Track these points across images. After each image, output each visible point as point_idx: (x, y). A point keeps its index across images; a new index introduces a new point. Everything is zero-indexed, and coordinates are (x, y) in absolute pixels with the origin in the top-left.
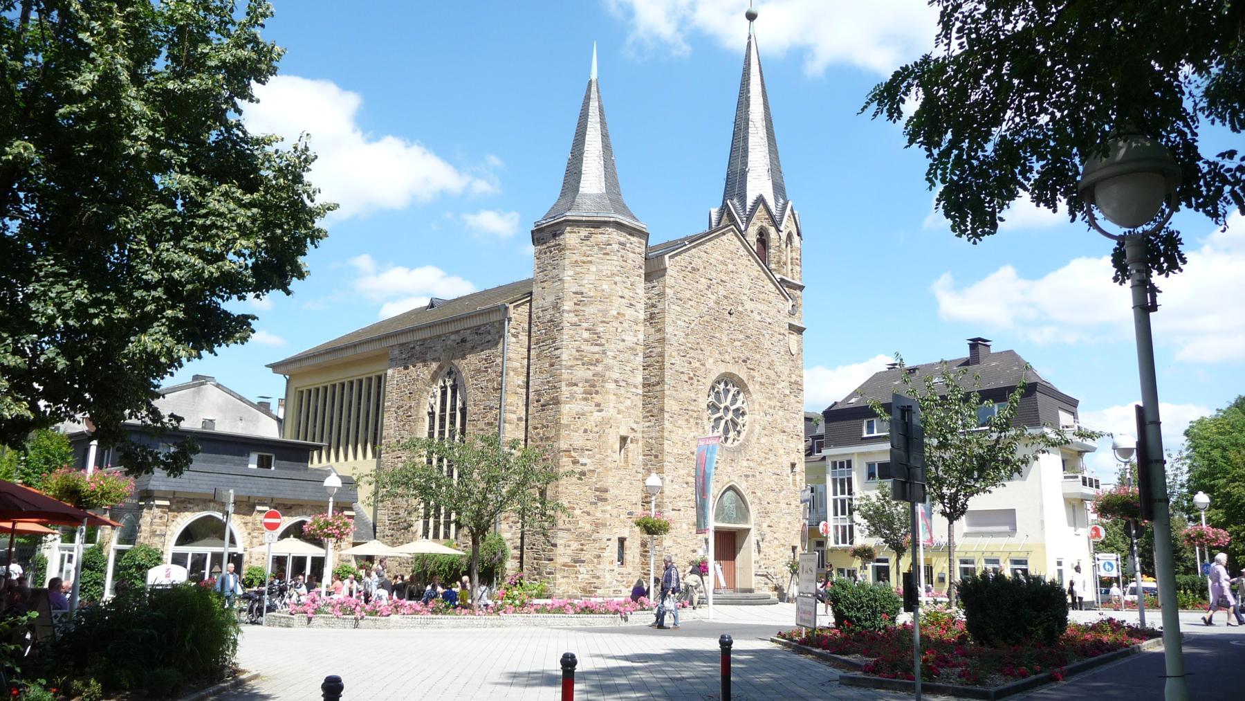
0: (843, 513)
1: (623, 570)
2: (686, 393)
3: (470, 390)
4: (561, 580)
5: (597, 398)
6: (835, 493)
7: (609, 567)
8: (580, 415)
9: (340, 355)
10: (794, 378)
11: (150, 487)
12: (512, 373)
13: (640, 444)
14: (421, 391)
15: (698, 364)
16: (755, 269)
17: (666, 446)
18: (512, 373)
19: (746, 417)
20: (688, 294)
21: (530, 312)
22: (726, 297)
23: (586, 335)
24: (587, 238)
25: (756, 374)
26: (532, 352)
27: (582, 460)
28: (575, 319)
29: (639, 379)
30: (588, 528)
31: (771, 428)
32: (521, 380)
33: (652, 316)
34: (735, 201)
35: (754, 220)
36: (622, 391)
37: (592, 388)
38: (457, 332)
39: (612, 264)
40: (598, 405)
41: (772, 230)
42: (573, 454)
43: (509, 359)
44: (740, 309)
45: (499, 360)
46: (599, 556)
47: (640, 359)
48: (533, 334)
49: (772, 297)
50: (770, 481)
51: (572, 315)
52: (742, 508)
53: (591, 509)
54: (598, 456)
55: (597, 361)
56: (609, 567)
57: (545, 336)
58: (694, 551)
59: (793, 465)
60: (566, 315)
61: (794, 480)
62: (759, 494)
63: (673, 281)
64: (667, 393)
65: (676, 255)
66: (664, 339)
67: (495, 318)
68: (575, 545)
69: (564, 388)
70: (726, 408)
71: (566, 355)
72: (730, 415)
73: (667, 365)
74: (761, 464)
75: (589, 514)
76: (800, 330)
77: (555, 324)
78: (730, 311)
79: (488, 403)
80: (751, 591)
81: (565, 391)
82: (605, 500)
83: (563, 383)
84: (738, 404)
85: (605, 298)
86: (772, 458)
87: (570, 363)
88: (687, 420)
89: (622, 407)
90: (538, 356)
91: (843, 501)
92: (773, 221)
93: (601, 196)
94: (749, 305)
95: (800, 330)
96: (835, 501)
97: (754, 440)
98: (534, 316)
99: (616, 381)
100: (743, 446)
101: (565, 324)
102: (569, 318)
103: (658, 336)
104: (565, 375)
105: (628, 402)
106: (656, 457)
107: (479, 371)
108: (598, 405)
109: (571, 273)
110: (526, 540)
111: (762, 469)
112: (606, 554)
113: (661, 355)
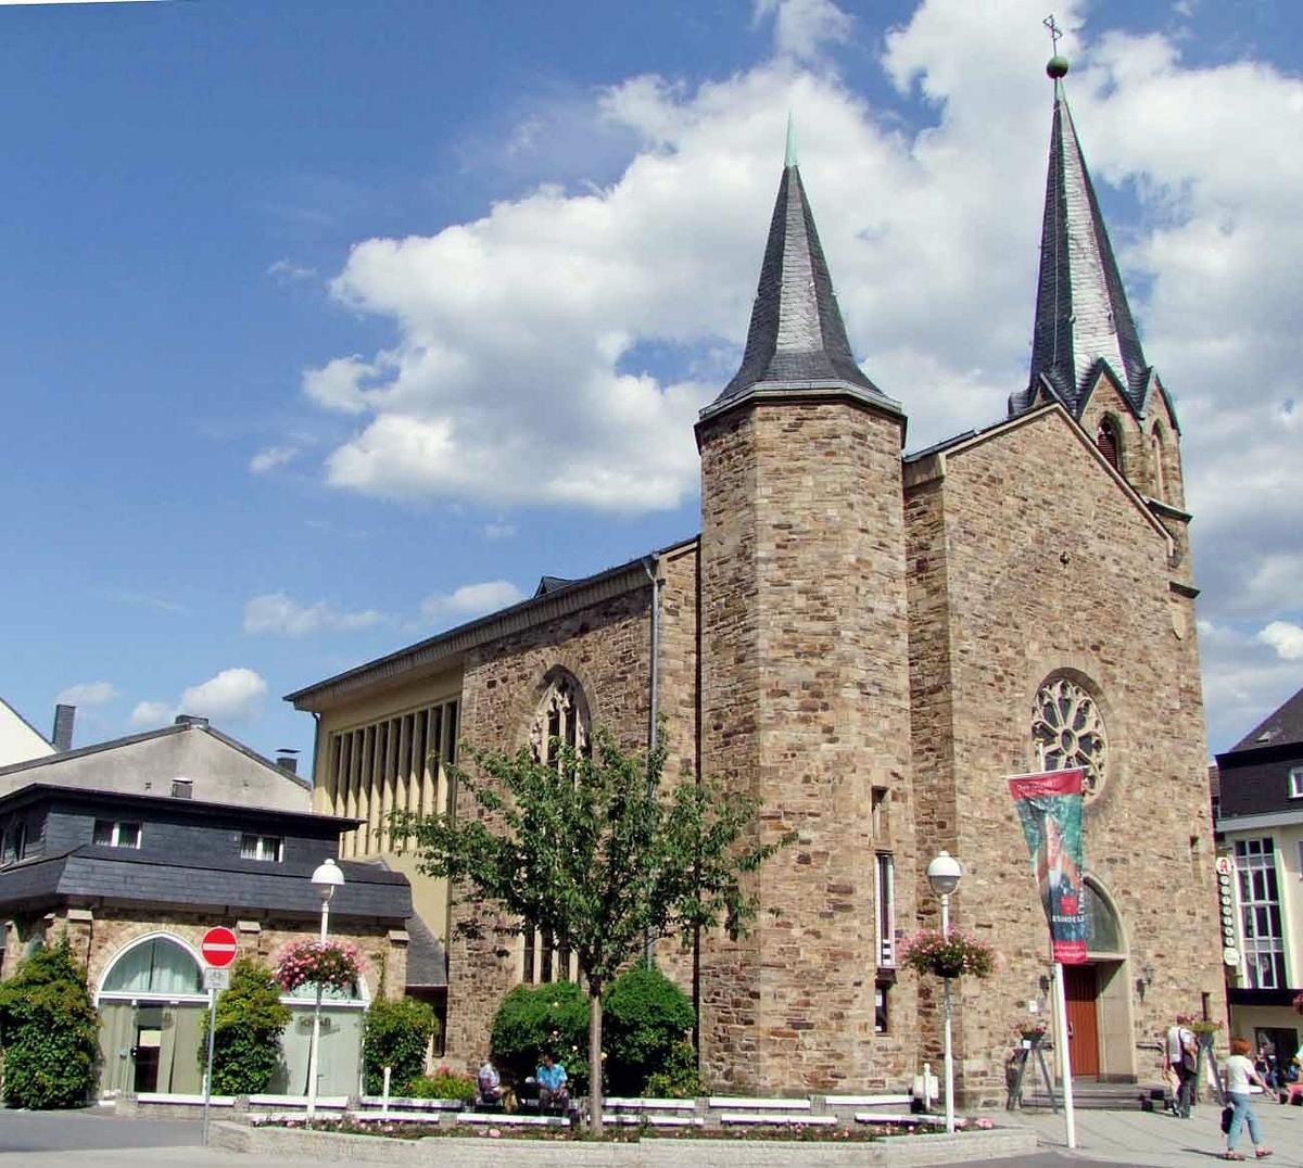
0: (1263, 931)
1: (886, 1041)
2: (993, 707)
3: (596, 715)
4: (770, 1062)
5: (827, 717)
6: (1245, 897)
7: (860, 1036)
8: (796, 750)
9: (389, 672)
10: (1184, 681)
11: (61, 890)
12: (668, 680)
13: (911, 801)
14: (517, 722)
15: (1010, 653)
16: (1103, 481)
17: (958, 806)
18: (668, 680)
19: (1104, 752)
20: (984, 524)
21: (698, 569)
22: (1054, 531)
23: (800, 602)
24: (795, 427)
25: (1117, 671)
26: (705, 640)
27: (804, 835)
28: (780, 574)
29: (902, 682)
30: (816, 961)
31: (1152, 771)
32: (686, 691)
33: (921, 566)
34: (1054, 375)
35: (1091, 402)
36: (873, 703)
37: (816, 699)
38: (572, 615)
39: (843, 473)
40: (828, 730)
41: (1126, 420)
42: (785, 822)
43: (664, 654)
44: (1081, 552)
45: (645, 658)
46: (841, 1016)
47: (902, 644)
48: (704, 608)
49: (1136, 533)
50: (1155, 870)
51: (773, 566)
52: (1106, 927)
53: (822, 925)
54: (832, 826)
55: (824, 648)
56: (860, 1036)
57: (725, 606)
58: (1021, 1004)
59: (1194, 841)
60: (761, 567)
61: (1196, 870)
62: (1136, 895)
63: (956, 500)
64: (957, 705)
65: (959, 452)
66: (945, 605)
67: (634, 583)
68: (793, 995)
69: (763, 701)
70: (1067, 734)
71: (764, 642)
72: (1075, 748)
73: (954, 653)
74: (1136, 837)
75: (817, 934)
76: (1190, 593)
77: (743, 587)
78: (1058, 556)
79: (628, 735)
80: (1131, 1079)
81: (766, 706)
82: (848, 908)
83: (763, 692)
84: (1089, 728)
85: (833, 533)
86: (1157, 827)
87: (773, 655)
88: (996, 756)
89: (873, 735)
90: (715, 646)
91: (1261, 911)
92: (1127, 402)
93: (814, 357)
94: (1096, 546)
95: (1190, 593)
96: (1246, 910)
97: (1120, 794)
98: (704, 575)
99: (861, 685)
100: (1101, 805)
101: (762, 585)
102: (767, 572)
103: (935, 601)
104: (765, 675)
105: (885, 725)
106: (942, 825)
107: (611, 680)
108: (828, 730)
109: (768, 491)
110: (702, 985)
111: (1138, 847)
112: (853, 1011)
113: (942, 635)
